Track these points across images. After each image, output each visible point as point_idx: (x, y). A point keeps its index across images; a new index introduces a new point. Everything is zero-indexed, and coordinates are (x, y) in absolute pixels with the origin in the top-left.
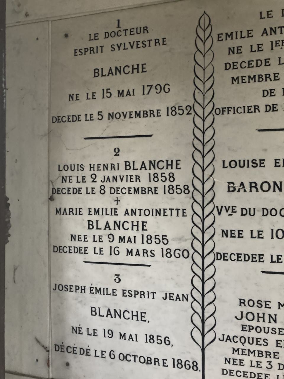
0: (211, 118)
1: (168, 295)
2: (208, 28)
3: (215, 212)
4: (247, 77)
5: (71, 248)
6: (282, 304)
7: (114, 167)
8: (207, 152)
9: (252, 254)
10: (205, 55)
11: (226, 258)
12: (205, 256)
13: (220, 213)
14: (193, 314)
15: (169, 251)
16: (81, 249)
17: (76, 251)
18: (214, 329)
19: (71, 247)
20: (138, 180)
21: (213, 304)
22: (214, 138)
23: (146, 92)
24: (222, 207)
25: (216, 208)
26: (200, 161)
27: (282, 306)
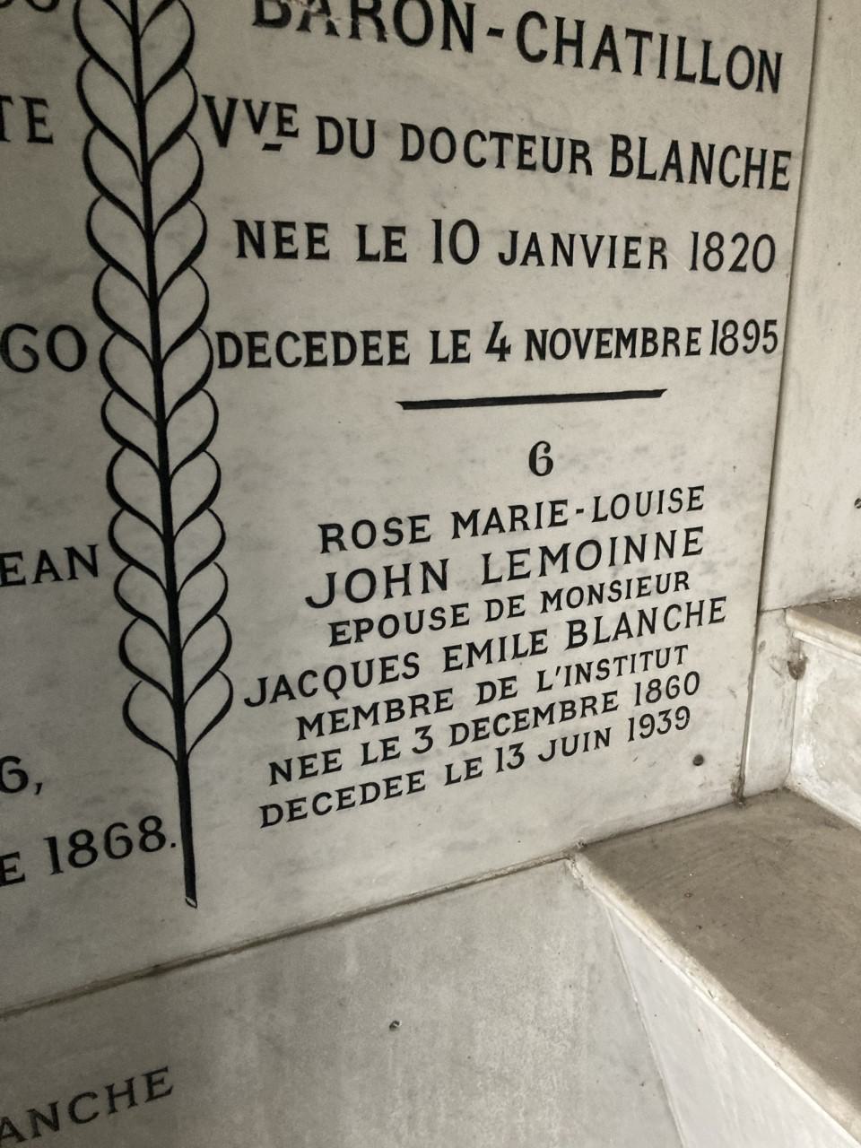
3: (202, 126)
7: (423, 706)
25: (202, 103)
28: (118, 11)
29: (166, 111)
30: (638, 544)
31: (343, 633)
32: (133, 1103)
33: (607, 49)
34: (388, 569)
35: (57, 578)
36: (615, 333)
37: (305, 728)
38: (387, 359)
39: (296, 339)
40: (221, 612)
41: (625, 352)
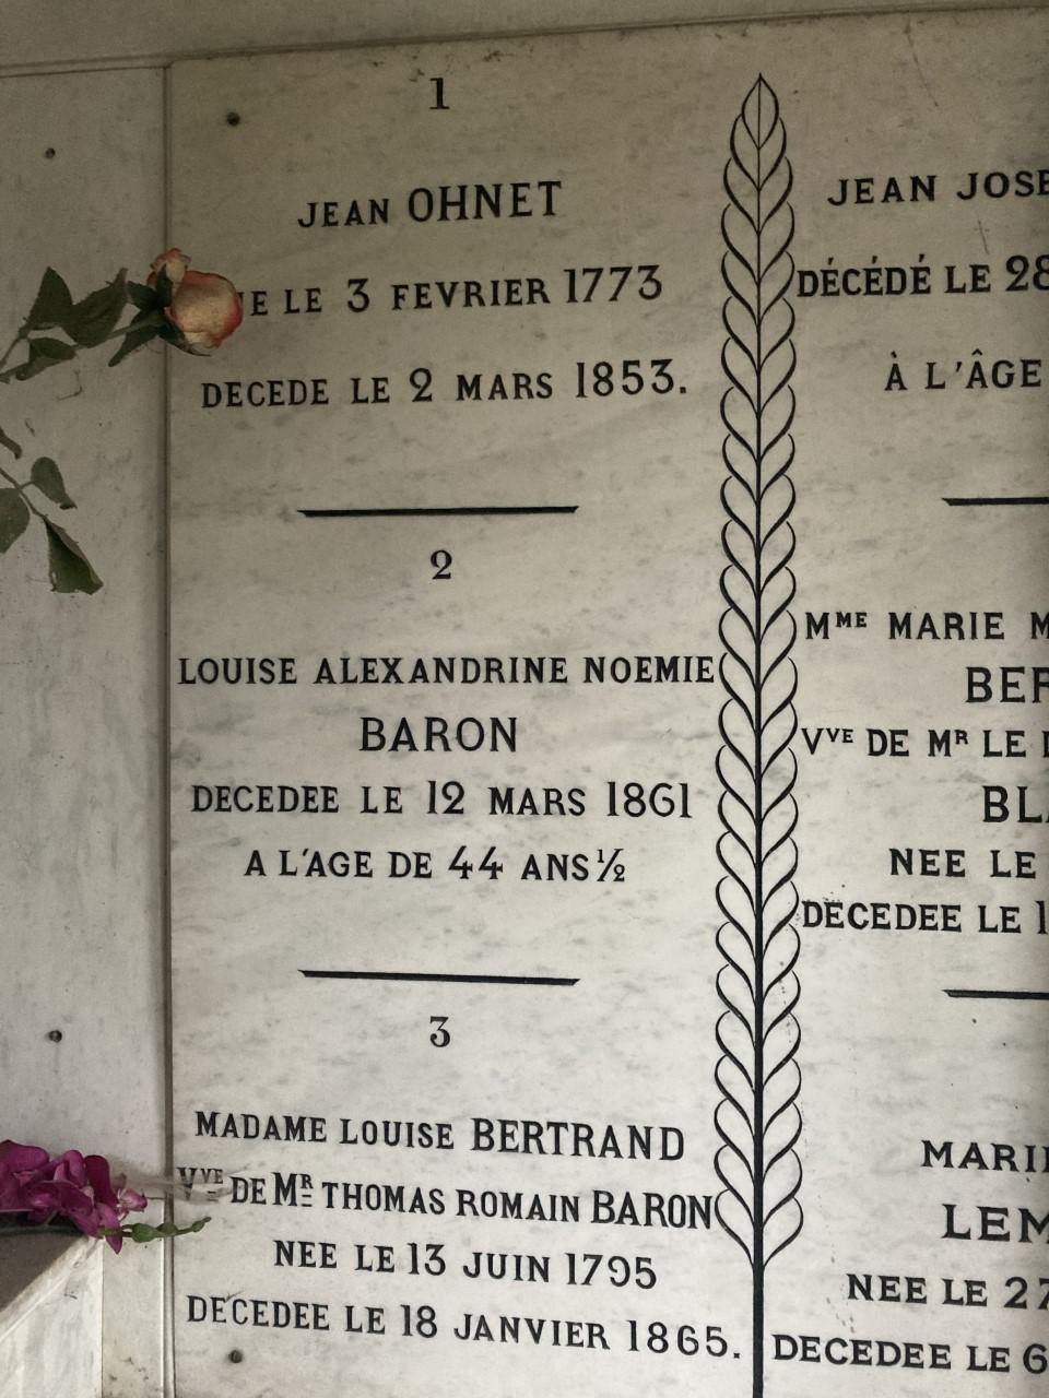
0: (782, 357)
2: (777, 215)
5: (277, 388)
6: (1039, 1218)
8: (767, 352)
9: (921, 906)
10: (760, 279)
11: (831, 288)
12: (764, 453)
13: (813, 748)
14: (723, 836)
15: (634, 792)
16: (312, 793)
18: (794, 1148)
19: (280, 383)
20: (537, 297)
21: (787, 569)
22: (791, 431)
23: (581, 1275)
24: (820, 731)
26: (747, 603)
27: (1039, 1228)
28: (749, 852)
29: (774, 735)
30: (485, 206)
31: (933, 862)
33: (498, 388)
34: (444, 190)
35: (935, 636)
36: (654, 661)
37: (931, 1155)
40: (797, 1196)
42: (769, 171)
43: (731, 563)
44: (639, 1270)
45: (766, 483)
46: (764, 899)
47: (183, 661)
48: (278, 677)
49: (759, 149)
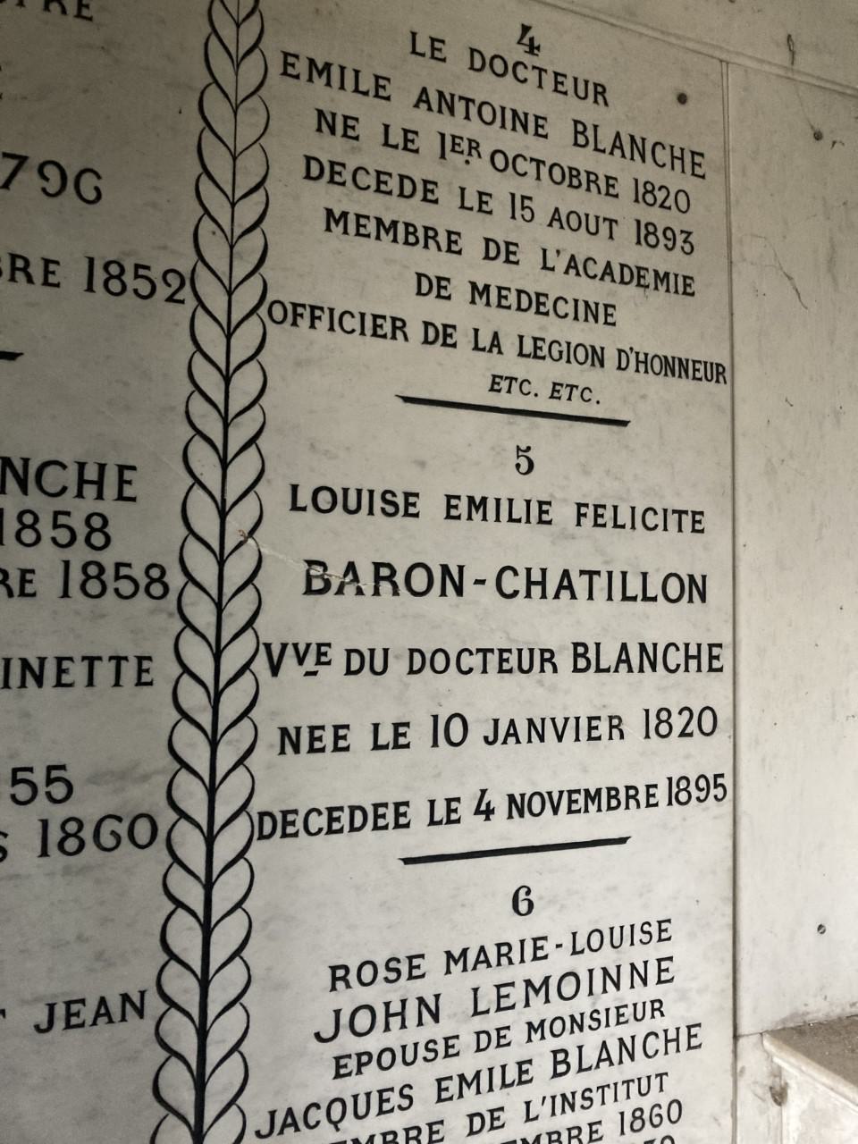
1: (60, 1011)
3: (261, 665)
4: (456, 1080)
17: (358, 823)
26: (212, 477)
29: (233, 659)
30: (614, 974)
32: (544, 596)
38: (392, 825)
39: (320, 813)
41: (593, 808)
42: (233, 547)
43: (166, 1112)
44: (118, 577)
45: (217, 967)
46: (208, 1070)
47: (683, 171)
48: (655, 937)
49: (235, 159)
